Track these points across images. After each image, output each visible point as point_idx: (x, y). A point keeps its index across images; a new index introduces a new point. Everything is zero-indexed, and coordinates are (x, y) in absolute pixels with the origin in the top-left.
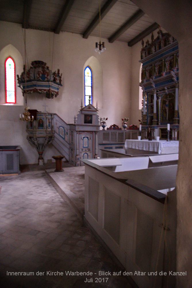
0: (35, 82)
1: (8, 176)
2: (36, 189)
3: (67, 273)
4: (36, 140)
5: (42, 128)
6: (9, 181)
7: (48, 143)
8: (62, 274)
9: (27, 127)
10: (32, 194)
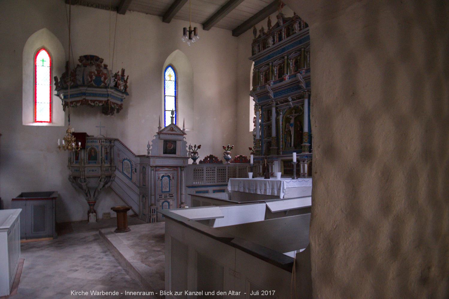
2: (83, 261)
5: (96, 163)
8: (86, 293)
9: (70, 160)
10: (77, 270)
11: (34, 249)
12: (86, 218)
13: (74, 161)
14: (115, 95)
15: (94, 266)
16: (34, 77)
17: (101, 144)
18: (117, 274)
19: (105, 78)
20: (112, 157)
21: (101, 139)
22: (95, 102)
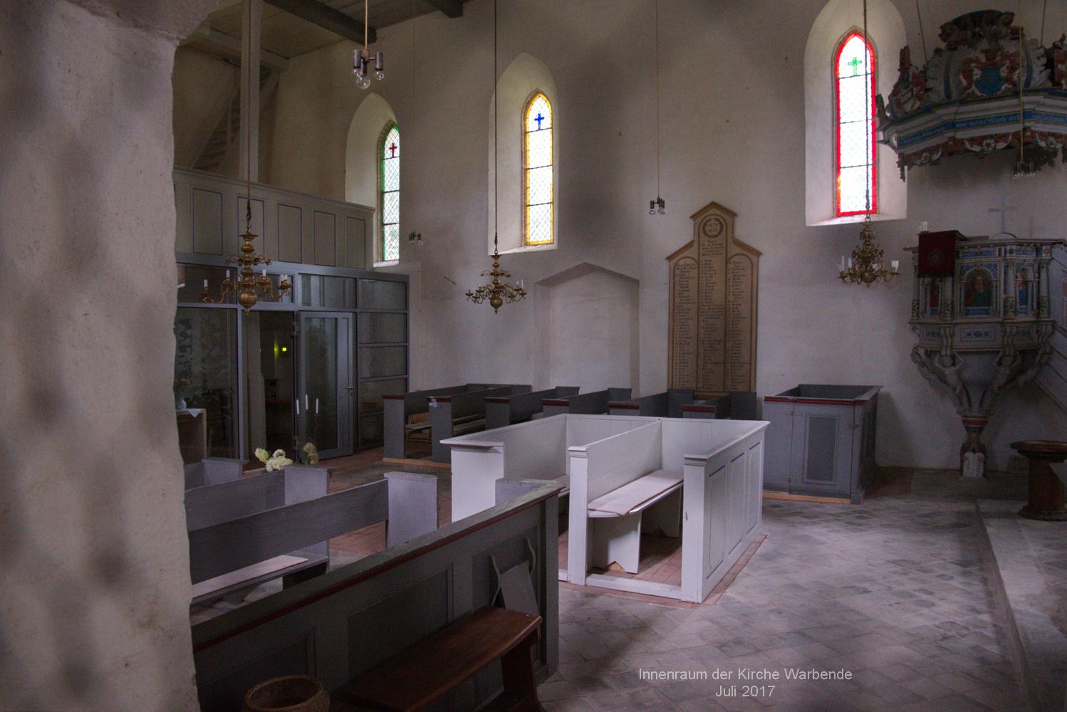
0: (952, 109)
1: (807, 504)
2: (895, 573)
3: (788, 674)
4: (954, 364)
5: (987, 313)
6: (806, 524)
7: (1012, 379)
9: (916, 307)
10: (866, 591)
11: (798, 519)
12: (957, 466)
13: (925, 309)
14: (1048, 110)
15: (917, 593)
16: (833, 108)
17: (1005, 259)
18: (966, 632)
19: (1012, 68)
20: (1044, 293)
21: (1005, 245)
22: (985, 142)
